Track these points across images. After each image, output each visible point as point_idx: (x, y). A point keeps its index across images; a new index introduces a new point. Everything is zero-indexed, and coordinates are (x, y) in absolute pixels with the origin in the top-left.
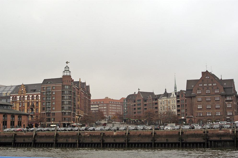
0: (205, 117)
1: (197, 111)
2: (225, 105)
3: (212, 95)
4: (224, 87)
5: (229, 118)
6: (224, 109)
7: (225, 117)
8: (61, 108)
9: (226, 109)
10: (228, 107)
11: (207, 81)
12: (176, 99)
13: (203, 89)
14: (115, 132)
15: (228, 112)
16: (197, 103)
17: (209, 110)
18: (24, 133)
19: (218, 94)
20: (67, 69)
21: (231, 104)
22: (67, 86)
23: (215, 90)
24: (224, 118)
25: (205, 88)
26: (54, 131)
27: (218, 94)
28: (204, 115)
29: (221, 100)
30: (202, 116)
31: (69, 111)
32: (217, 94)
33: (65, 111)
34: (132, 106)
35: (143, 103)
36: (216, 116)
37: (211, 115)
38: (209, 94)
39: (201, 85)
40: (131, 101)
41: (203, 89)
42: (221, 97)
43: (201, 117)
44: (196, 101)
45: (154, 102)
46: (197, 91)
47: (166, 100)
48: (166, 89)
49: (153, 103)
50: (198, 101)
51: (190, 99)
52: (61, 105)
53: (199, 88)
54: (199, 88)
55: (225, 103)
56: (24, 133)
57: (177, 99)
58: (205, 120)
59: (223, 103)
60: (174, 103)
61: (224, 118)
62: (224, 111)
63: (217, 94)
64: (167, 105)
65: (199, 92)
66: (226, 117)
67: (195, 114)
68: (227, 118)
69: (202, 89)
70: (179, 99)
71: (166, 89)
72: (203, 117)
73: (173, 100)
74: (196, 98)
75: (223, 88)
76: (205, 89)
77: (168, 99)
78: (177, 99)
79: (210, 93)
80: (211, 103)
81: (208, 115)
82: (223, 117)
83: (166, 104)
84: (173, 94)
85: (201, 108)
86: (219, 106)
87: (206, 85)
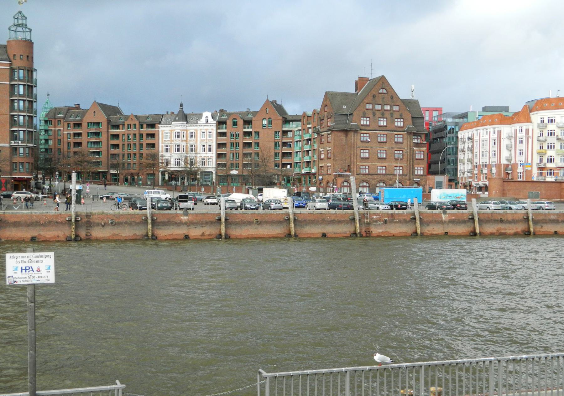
0: (375, 177)
1: (360, 162)
2: (413, 154)
3: (390, 129)
4: (415, 116)
5: (419, 180)
6: (410, 162)
7: (411, 178)
8: (8, 134)
9: (413, 161)
10: (417, 157)
11: (383, 99)
12: (214, 128)
13: (374, 114)
14: (445, 213)
15: (416, 168)
16: (359, 144)
17: (382, 163)
18: (181, 215)
19: (400, 129)
20: (20, 22)
21: (422, 152)
22: (21, 71)
23: (396, 120)
24: (410, 180)
25: (378, 114)
26: (239, 209)
27: (400, 129)
28: (372, 172)
29: (405, 142)
30: (369, 174)
31: (30, 143)
32: (399, 129)
33: (22, 143)
34: (65, 136)
35: (108, 132)
36: (377, 174)
37: (384, 172)
38: (385, 129)
39: (370, 107)
40: (66, 124)
41: (374, 114)
42: (406, 137)
43: (367, 176)
44: (359, 141)
45: (145, 130)
46: (362, 119)
47: (184, 130)
48: (181, 105)
49: (141, 133)
50: (362, 142)
51: (342, 136)
52: (8, 125)
53: (366, 111)
54: (366, 111)
55: (413, 150)
56: (181, 215)
57: (219, 129)
58: (373, 182)
59: (410, 149)
60: (208, 138)
61: (410, 180)
62: (410, 166)
63: (398, 129)
64: (186, 141)
65: (365, 122)
66: (413, 178)
67: (355, 169)
68: (415, 179)
69: (371, 116)
70: (251, 128)
71: (181, 105)
72: (370, 177)
73: (206, 130)
74: (359, 134)
75: (413, 118)
76: (377, 116)
77: (188, 128)
78: (218, 128)
79: (386, 126)
80: (386, 147)
81: (379, 172)
82: (407, 177)
83: (185, 139)
84: (207, 117)
85: (367, 155)
86: (385, 155)
87: (389, 108)
